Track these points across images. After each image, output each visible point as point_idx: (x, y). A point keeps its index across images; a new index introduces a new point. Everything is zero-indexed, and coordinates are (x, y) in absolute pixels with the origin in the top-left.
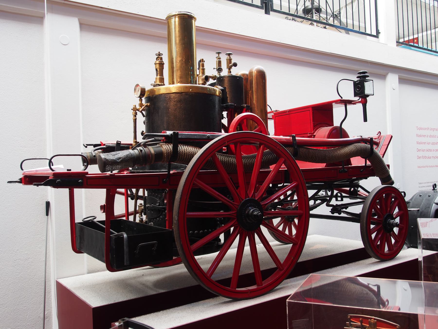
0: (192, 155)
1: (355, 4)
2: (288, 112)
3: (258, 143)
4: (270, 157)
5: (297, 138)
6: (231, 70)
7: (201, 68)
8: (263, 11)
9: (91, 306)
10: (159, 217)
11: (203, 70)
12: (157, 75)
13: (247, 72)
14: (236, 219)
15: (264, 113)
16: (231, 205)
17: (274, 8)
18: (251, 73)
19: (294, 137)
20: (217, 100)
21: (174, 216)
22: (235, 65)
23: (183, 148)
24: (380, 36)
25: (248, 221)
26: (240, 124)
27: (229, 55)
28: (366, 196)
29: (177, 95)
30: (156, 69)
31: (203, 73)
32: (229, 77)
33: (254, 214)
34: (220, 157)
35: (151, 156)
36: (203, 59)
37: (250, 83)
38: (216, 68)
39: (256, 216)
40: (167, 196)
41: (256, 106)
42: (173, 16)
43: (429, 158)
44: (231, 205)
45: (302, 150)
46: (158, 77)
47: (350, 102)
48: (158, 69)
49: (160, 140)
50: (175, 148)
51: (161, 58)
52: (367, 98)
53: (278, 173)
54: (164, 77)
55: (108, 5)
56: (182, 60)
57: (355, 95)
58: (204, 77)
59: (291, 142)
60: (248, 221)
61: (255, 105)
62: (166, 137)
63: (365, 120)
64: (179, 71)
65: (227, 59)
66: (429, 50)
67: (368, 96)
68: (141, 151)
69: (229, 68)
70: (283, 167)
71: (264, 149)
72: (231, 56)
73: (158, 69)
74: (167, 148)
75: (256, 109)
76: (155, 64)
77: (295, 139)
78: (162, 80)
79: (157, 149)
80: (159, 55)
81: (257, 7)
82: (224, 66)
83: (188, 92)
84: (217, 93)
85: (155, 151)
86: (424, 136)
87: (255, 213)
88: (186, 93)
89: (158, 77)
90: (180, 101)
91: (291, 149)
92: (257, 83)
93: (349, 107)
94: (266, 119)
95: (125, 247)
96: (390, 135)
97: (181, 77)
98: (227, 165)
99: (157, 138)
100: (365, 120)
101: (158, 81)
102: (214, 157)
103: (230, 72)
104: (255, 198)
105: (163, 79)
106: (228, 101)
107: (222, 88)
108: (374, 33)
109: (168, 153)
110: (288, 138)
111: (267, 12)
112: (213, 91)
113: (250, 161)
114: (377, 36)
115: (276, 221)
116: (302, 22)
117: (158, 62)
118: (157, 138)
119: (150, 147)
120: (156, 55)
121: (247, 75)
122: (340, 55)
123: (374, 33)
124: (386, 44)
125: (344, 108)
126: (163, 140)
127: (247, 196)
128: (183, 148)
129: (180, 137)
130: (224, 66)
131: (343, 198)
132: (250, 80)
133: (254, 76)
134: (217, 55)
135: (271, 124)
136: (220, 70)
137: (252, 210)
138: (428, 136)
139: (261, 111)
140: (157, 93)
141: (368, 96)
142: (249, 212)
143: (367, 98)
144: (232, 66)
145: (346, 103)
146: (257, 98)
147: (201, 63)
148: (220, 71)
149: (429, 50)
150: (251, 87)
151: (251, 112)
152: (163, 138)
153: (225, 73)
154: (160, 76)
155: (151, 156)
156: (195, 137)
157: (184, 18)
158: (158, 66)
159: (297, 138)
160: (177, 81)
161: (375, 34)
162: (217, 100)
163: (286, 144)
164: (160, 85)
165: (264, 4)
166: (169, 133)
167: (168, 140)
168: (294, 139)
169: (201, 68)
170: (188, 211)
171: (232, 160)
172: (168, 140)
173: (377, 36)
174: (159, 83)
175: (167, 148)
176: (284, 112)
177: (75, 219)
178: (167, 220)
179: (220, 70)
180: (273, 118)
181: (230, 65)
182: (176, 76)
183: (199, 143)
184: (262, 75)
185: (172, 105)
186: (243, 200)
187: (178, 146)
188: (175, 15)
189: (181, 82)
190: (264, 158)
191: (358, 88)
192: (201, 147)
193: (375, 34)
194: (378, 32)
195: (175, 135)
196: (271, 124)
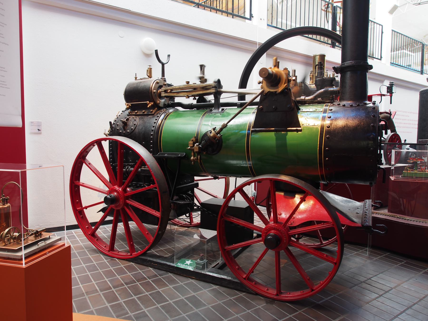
1: (285, 2)
9: (197, 196)
24: (382, 59)
28: (384, 139)
43: (400, 127)
47: (384, 95)
52: (393, 94)
55: (109, 3)
57: (388, 92)
63: (391, 103)
66: (403, 67)
67: (393, 93)
86: (399, 115)
93: (383, 97)
96: (395, 111)
100: (391, 103)
101: (311, 82)
108: (379, 58)
114: (380, 60)
116: (320, 44)
122: (122, 9)
123: (379, 58)
124: (385, 64)
125: (380, 97)
131: (104, 214)
138: (401, 115)
141: (393, 93)
143: (393, 94)
145: (382, 95)
149: (403, 67)
161: (380, 59)
173: (380, 60)
188: (318, 55)
191: (389, 89)
193: (380, 59)
194: (381, 57)
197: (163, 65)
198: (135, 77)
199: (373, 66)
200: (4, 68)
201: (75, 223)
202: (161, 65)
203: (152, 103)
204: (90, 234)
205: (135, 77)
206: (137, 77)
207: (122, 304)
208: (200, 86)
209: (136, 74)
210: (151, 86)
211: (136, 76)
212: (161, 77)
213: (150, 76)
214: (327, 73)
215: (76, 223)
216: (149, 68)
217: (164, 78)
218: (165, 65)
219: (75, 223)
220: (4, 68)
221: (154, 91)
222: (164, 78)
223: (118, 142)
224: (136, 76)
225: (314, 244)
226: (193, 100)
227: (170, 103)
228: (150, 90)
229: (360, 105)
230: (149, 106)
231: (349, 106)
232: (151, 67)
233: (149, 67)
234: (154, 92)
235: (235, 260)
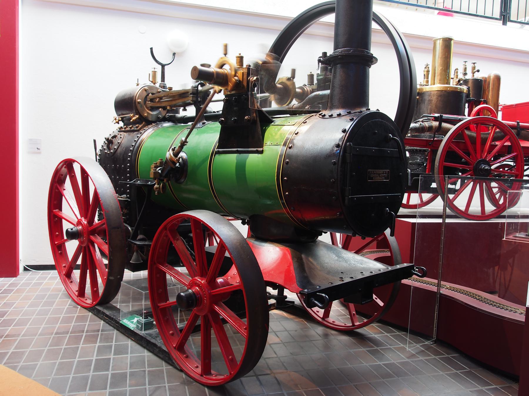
0: (448, 130)
2: (515, 105)
3: (492, 124)
4: (499, 134)
5: (520, 124)
6: (475, 74)
7: (456, 74)
8: (502, 22)
10: (418, 169)
11: (457, 75)
12: (424, 79)
13: (486, 76)
14: (473, 171)
15: (496, 105)
16: (470, 161)
17: (511, 19)
18: (489, 77)
19: (518, 123)
20: (464, 96)
21: (435, 163)
22: (478, 71)
23: (445, 125)
25: (481, 173)
26: (478, 113)
27: (474, 63)
29: (437, 92)
30: (424, 75)
31: (457, 77)
32: (473, 79)
33: (486, 168)
34: (467, 132)
35: (426, 128)
36: (457, 69)
37: (488, 84)
38: (462, 72)
39: (487, 169)
40: (429, 154)
41: (491, 100)
42: (439, 39)
44: (470, 161)
45: (523, 132)
46: (425, 80)
48: (426, 75)
49: (430, 119)
50: (440, 124)
51: (429, 68)
53: (503, 147)
54: (429, 80)
56: (443, 69)
58: (458, 80)
59: (516, 126)
60: (481, 173)
61: (490, 100)
62: (435, 117)
64: (439, 76)
65: (472, 67)
68: (421, 124)
69: (473, 73)
70: (508, 144)
71: (495, 129)
72: (475, 64)
73: (426, 75)
74: (436, 124)
75: (490, 102)
76: (424, 71)
77: (519, 124)
78: (427, 82)
79: (430, 124)
80: (427, 65)
81: (496, 19)
82: (469, 71)
83: (446, 90)
84: (465, 91)
85: (428, 125)
87: (486, 168)
88: (445, 91)
89: (425, 80)
90: (440, 96)
91: (516, 131)
92: (493, 85)
94: (497, 111)
95: (409, 176)
97: (440, 80)
98: (470, 137)
99: (429, 118)
102: (463, 132)
103: (474, 76)
104: (486, 159)
105: (428, 81)
106: (471, 97)
107: (467, 87)
109: (436, 127)
110: (514, 123)
111: (504, 23)
112: (463, 90)
113: (485, 136)
115: (494, 184)
117: (426, 70)
118: (429, 118)
119: (425, 123)
120: (425, 65)
121: (486, 78)
126: (432, 119)
127: (481, 157)
128: (444, 125)
129: (443, 118)
130: (469, 71)
132: (488, 82)
133: (492, 79)
134: (464, 63)
135: (500, 114)
136: (465, 74)
137: (483, 166)
139: (494, 105)
140: (424, 90)
142: (481, 167)
144: (475, 72)
146: (492, 95)
147: (456, 71)
148: (466, 75)
150: (489, 87)
151: (486, 104)
152: (433, 118)
153: (469, 76)
154: (427, 79)
155: (426, 128)
156: (452, 119)
157: (446, 41)
158: (425, 73)
159: (520, 124)
160: (437, 82)
162: (464, 96)
163: (513, 127)
164: (426, 85)
165: (502, 16)
166: (437, 115)
167: (436, 119)
168: (518, 124)
169: (456, 74)
170: (445, 162)
171: (474, 134)
172: (436, 119)
174: (425, 84)
175: (436, 124)
176: (511, 106)
177: (453, 132)
178: (427, 168)
179: (465, 74)
180: (502, 110)
181: (474, 71)
182: (437, 78)
183: (453, 122)
184: (498, 79)
185: (434, 99)
186: (478, 159)
187: (441, 124)
188: (440, 39)
189: (440, 83)
190: (495, 135)
192: (455, 125)
195: (441, 116)
196: (500, 114)
197: (163, 66)
198: (137, 84)
199: (197, 66)
200: (150, 74)
201: (52, 262)
202: (160, 67)
203: (137, 116)
204: (175, 348)
205: (137, 84)
206: (139, 83)
207: (100, 374)
208: (173, 93)
209: (138, 79)
210: (135, 95)
211: (138, 82)
212: (160, 83)
213: (154, 82)
214: (466, 66)
215: (54, 264)
216: (153, 71)
217: (164, 83)
218: (166, 67)
219: (52, 262)
220: (150, 74)
221: (139, 100)
222: (164, 83)
223: (104, 166)
224: (138, 82)
225: (345, 324)
226: (183, 111)
227: (168, 115)
228: (134, 99)
229: (352, 112)
230: (133, 120)
231: (347, 114)
232: (156, 70)
233: (153, 70)
234: (139, 103)
235: (223, 326)
